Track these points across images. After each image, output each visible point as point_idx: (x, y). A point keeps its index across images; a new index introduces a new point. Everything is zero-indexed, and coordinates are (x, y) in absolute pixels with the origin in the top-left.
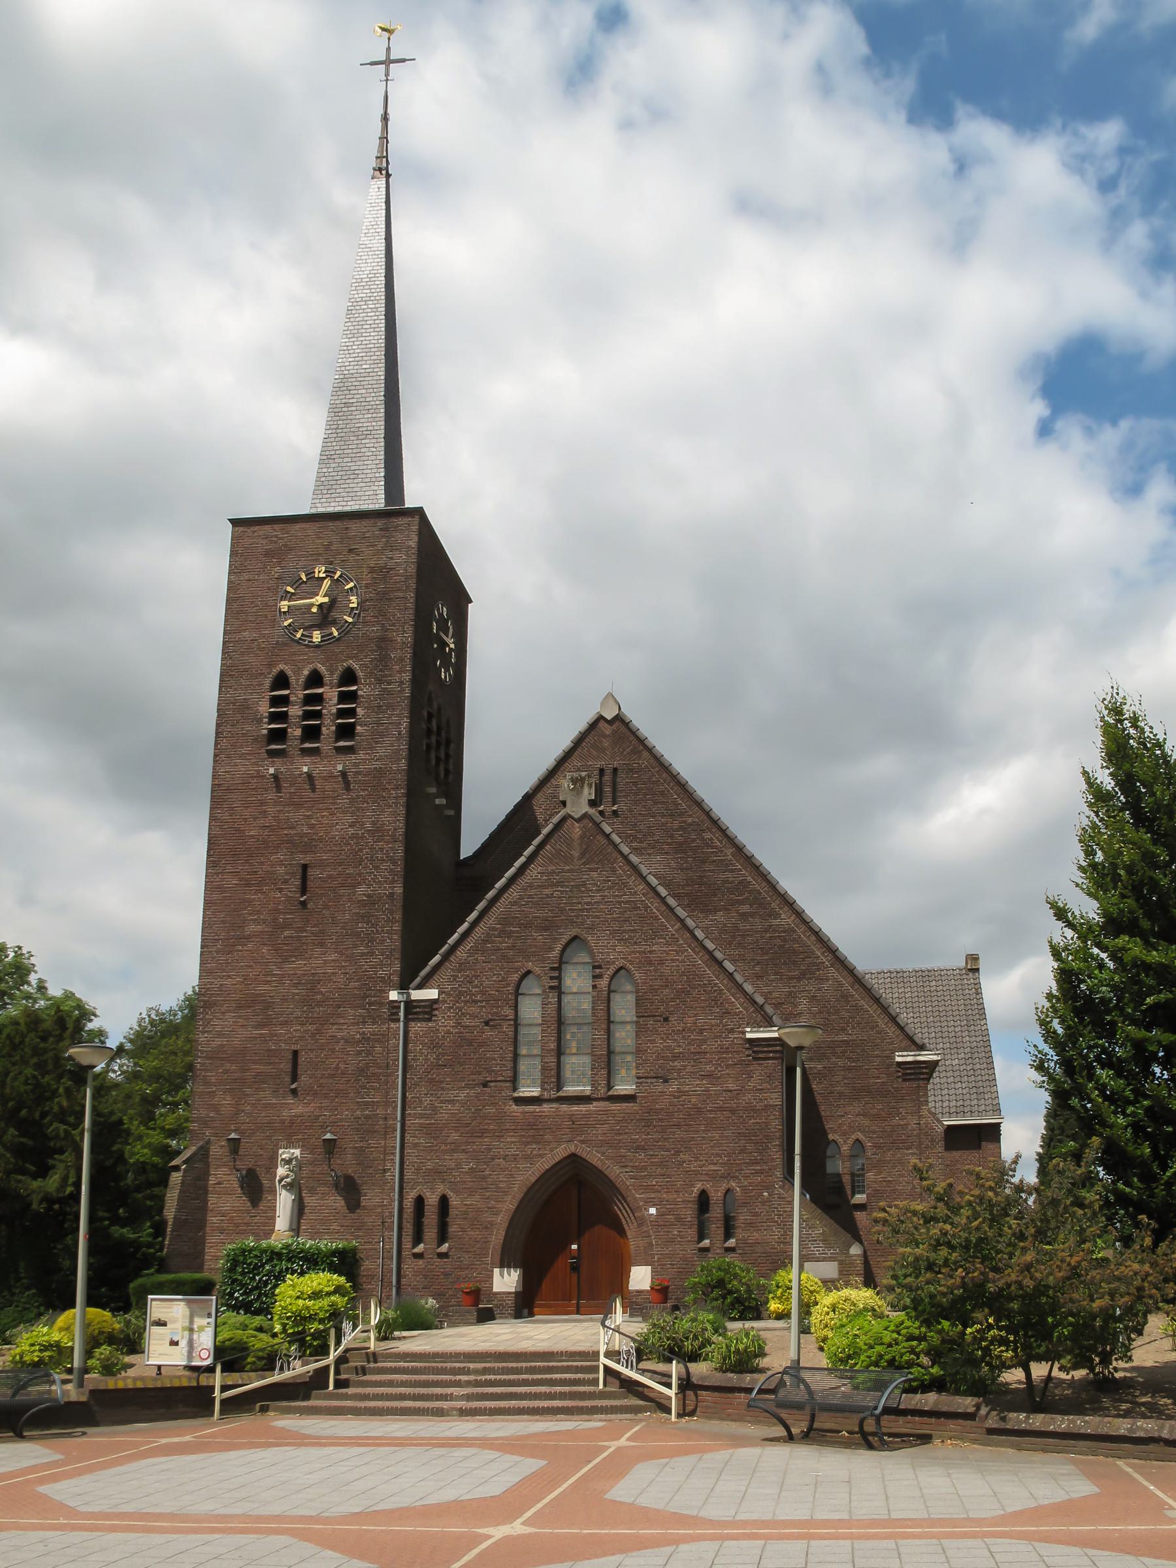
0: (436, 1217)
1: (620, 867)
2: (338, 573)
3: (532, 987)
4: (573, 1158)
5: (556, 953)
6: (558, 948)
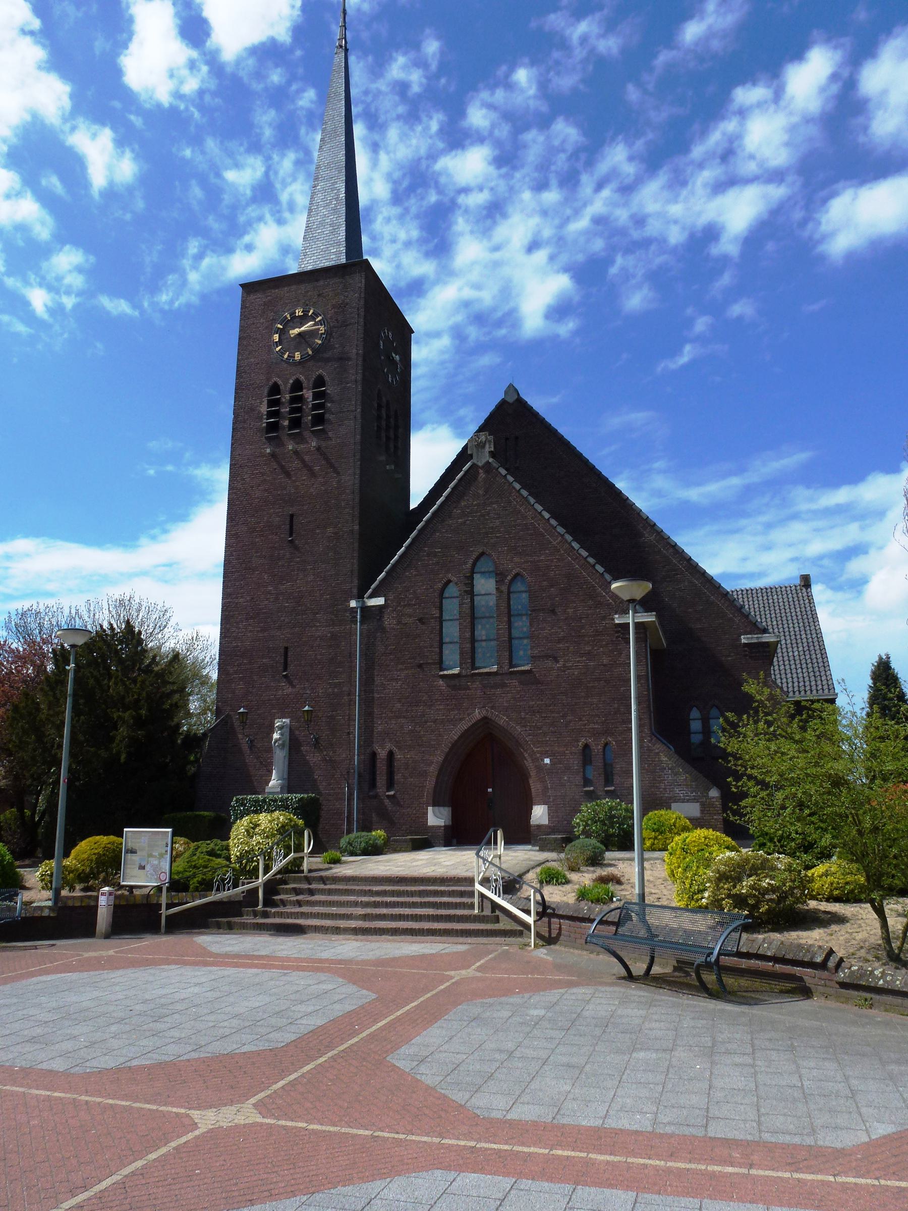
0: (385, 768)
1: (514, 499)
2: (311, 312)
3: (452, 590)
4: (485, 720)
5: (469, 566)
6: (471, 561)
